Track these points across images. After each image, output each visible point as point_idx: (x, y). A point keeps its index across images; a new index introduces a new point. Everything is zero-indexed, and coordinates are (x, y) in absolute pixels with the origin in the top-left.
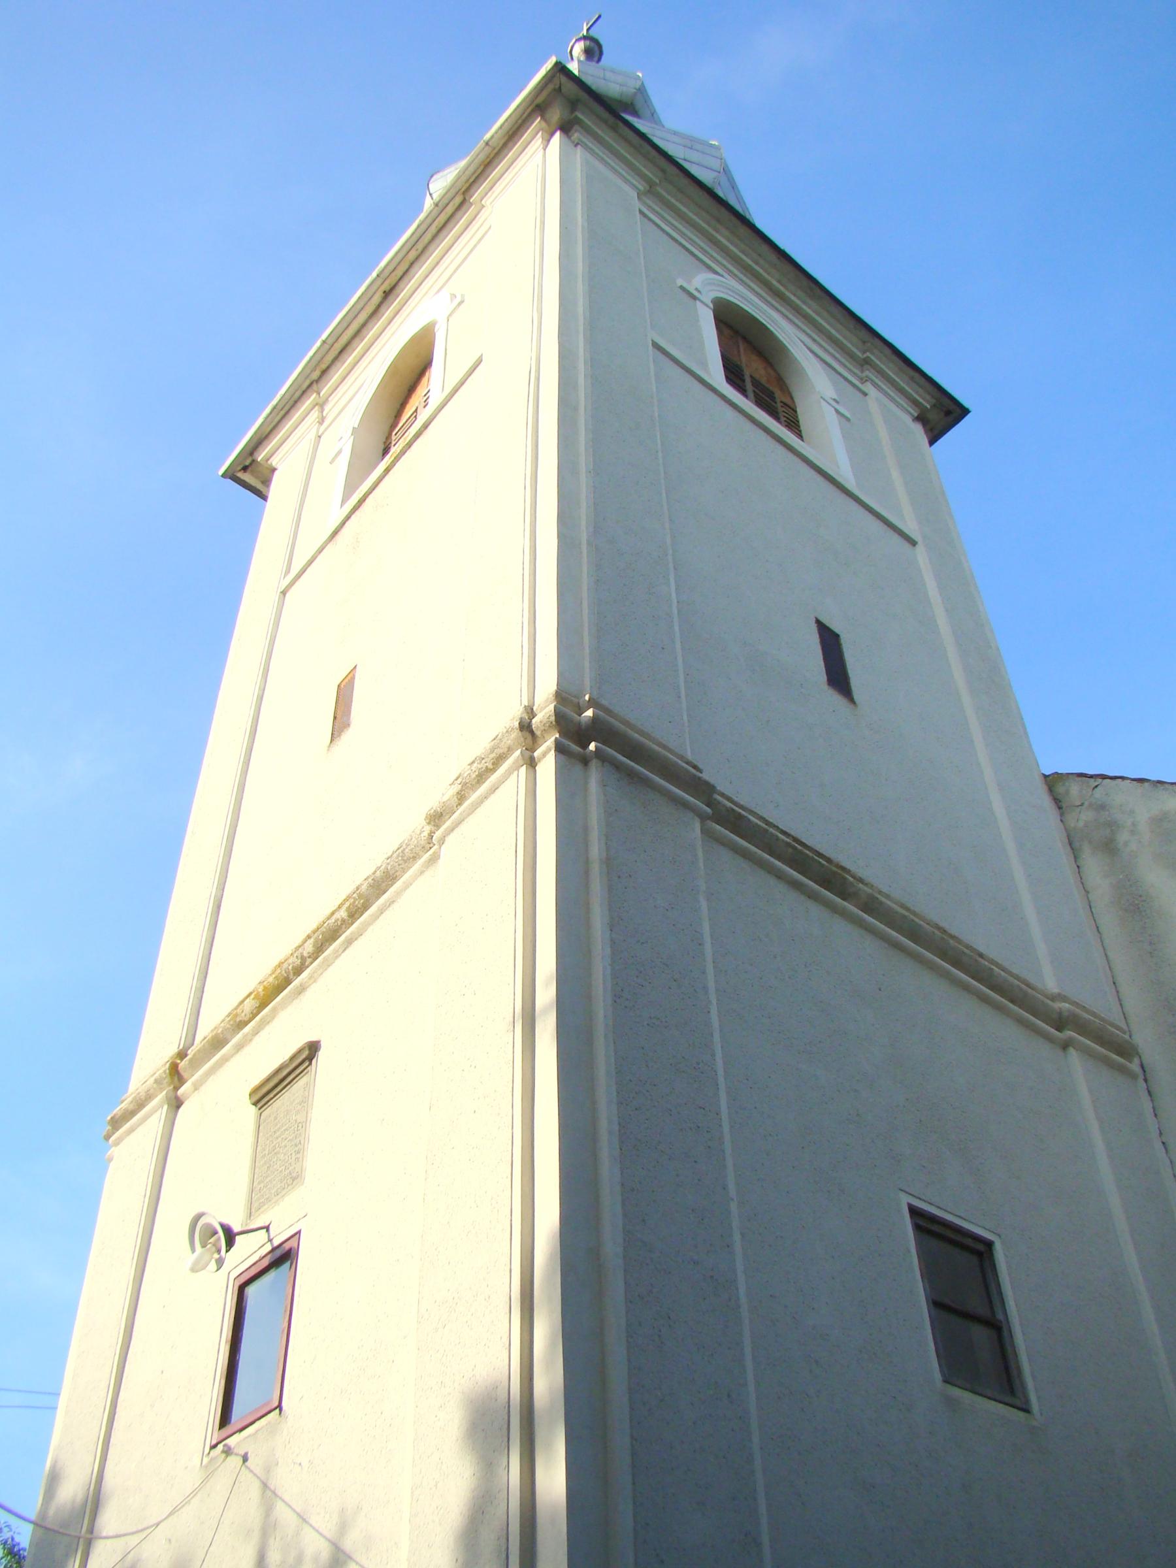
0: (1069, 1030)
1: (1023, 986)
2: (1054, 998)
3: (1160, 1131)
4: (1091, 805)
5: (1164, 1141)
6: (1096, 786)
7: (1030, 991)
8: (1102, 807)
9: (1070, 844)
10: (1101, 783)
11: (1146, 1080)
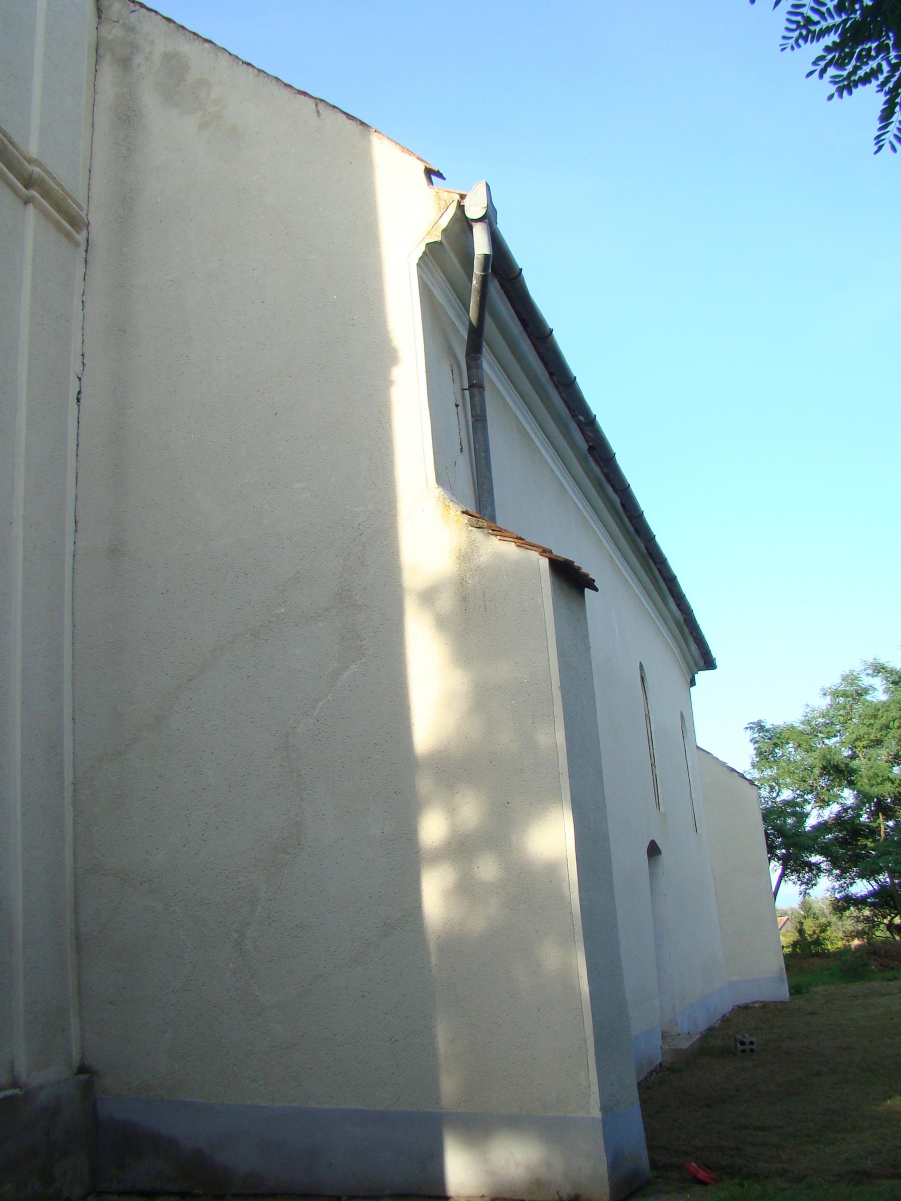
0: (34, 190)
1: (6, 142)
2: (30, 161)
3: (84, 292)
4: (123, 25)
5: (84, 300)
6: (134, 11)
7: (10, 147)
8: (131, 30)
9: (97, 51)
10: (138, 10)
11: (86, 251)
